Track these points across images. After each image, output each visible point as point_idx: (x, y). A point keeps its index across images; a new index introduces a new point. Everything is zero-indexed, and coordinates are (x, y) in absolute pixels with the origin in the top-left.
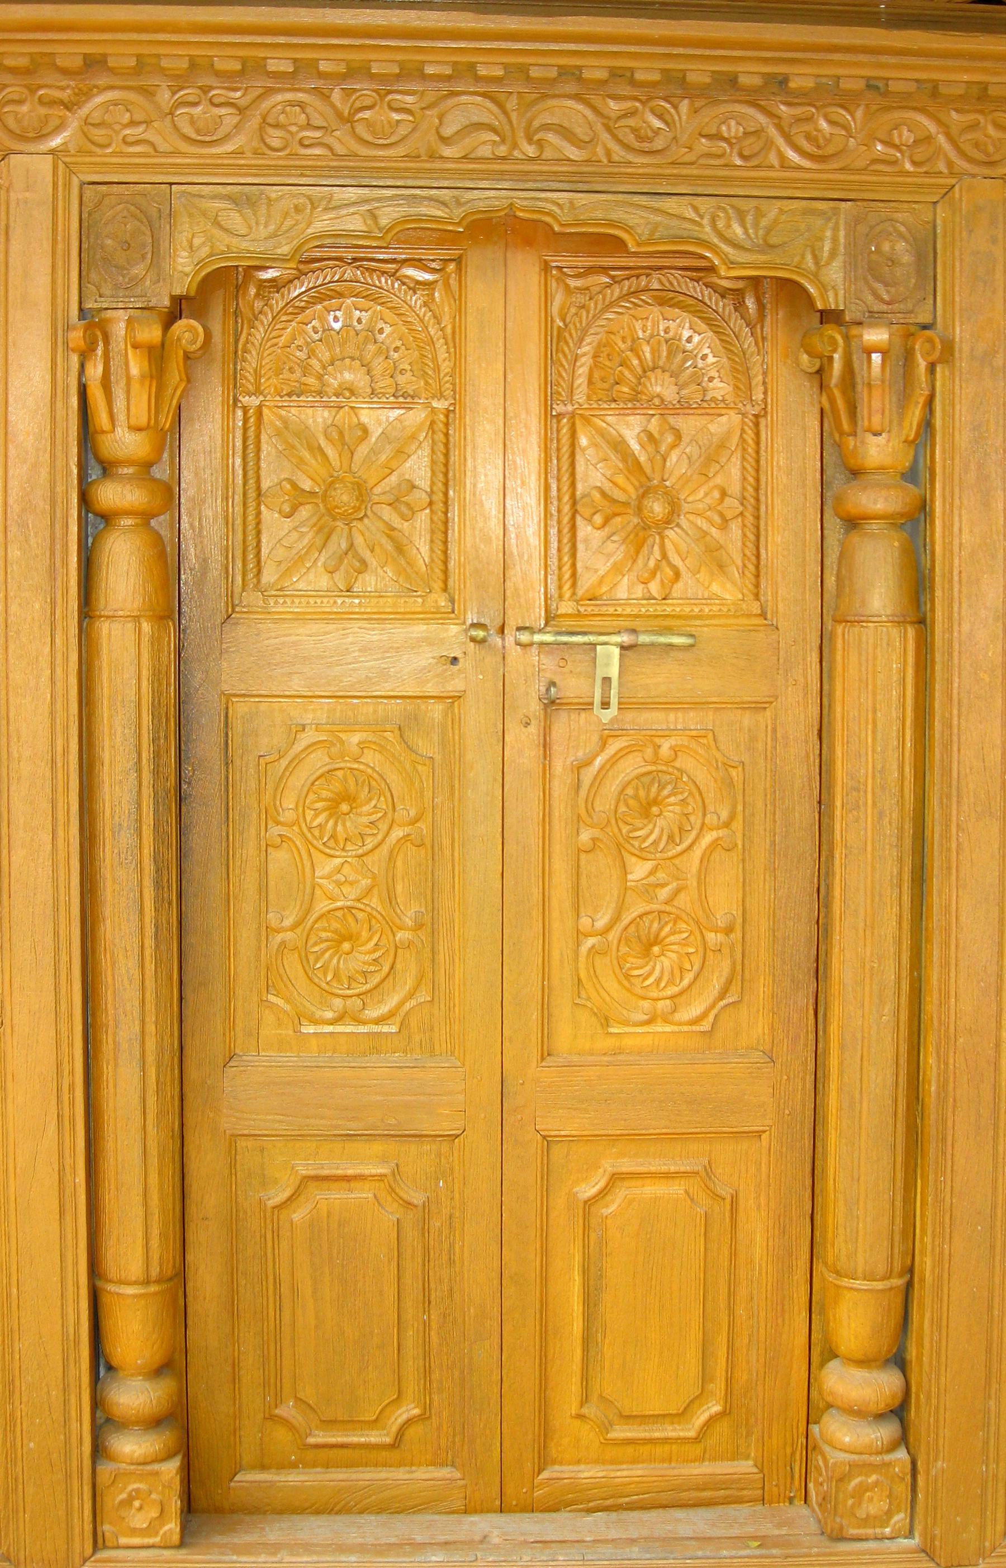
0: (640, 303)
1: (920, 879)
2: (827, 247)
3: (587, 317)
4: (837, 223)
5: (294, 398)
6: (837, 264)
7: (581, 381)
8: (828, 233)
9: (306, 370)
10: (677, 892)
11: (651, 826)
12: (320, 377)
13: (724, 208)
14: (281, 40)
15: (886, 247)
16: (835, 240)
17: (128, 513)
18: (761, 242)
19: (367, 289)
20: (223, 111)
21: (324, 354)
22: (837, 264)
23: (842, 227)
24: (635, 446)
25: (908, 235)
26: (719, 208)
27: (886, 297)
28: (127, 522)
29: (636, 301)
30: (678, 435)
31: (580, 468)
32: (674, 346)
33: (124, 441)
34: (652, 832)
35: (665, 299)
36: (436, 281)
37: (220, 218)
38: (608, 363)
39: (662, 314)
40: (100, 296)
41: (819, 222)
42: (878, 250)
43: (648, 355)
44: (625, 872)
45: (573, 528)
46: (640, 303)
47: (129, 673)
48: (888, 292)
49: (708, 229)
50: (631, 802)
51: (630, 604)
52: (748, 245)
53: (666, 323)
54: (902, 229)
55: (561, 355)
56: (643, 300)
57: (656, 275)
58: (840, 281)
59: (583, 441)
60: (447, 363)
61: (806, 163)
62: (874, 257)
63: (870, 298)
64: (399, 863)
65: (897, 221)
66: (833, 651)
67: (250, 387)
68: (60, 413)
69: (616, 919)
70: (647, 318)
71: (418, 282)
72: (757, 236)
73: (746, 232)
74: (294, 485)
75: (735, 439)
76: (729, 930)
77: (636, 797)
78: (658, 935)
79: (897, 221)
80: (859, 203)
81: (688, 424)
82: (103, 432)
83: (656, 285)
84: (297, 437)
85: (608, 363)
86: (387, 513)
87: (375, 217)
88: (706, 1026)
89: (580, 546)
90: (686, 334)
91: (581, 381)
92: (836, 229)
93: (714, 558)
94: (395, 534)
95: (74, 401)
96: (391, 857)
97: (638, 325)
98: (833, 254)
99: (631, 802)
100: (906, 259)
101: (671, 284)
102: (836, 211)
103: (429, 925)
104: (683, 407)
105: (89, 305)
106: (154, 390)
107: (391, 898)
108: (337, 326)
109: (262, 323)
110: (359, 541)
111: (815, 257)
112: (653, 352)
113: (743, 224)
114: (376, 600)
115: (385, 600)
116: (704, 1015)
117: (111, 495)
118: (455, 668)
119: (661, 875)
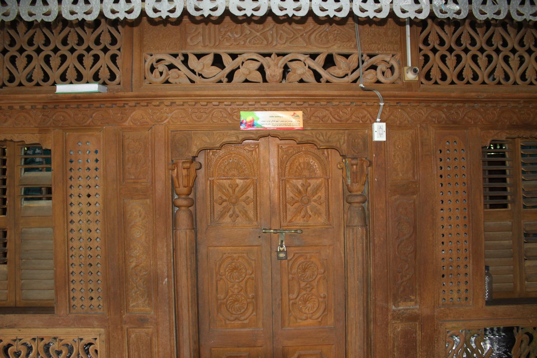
1: (198, 320)
2: (343, 141)
6: (345, 145)
10: (312, 289)
12: (227, 173)
14: (216, 98)
15: (356, 141)
16: (344, 139)
17: (183, 206)
20: (203, 114)
21: (227, 167)
22: (345, 145)
24: (300, 187)
28: (183, 208)
31: (287, 192)
32: (308, 164)
35: (307, 153)
41: (341, 135)
44: (300, 284)
45: (286, 206)
59: (288, 186)
61: (338, 122)
63: (353, 152)
66: (347, 299)
69: (298, 296)
74: (222, 198)
75: (323, 185)
76: (325, 297)
83: (304, 150)
84: (221, 187)
86: (243, 204)
87: (238, 138)
88: (320, 320)
89: (288, 210)
90: (311, 160)
92: (344, 136)
95: (170, 181)
96: (246, 282)
98: (344, 143)
100: (361, 143)
102: (345, 133)
103: (255, 297)
107: (246, 292)
108: (231, 161)
110: (237, 210)
111: (340, 143)
113: (323, 136)
116: (319, 317)
118: (259, 239)
119: (308, 286)
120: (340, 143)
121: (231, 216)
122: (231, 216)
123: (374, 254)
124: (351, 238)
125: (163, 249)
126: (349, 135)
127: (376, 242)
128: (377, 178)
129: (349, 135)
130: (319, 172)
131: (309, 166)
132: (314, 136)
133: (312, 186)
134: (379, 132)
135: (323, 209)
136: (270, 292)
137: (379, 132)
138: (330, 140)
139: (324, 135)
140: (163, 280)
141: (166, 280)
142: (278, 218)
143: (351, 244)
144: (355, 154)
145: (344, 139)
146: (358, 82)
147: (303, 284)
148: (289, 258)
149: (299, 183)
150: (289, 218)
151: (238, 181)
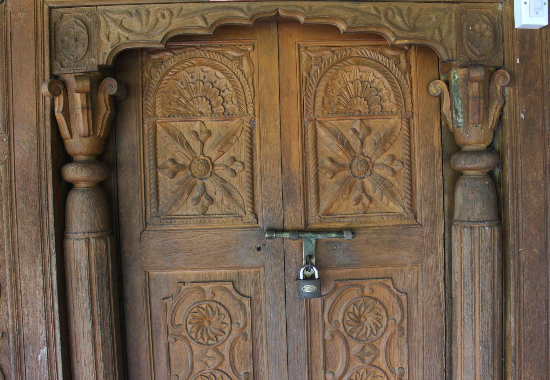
0: (347, 64)
3: (321, 72)
4: (451, 15)
5: (172, 118)
7: (319, 104)
8: (446, 20)
9: (178, 102)
11: (361, 327)
13: (392, 8)
15: (477, 27)
16: (450, 24)
18: (412, 26)
19: (209, 61)
23: (453, 16)
25: (488, 21)
26: (389, 8)
27: (478, 53)
29: (345, 63)
30: (369, 130)
33: (78, 143)
34: (362, 330)
36: (243, 56)
37: (123, 23)
38: (332, 94)
39: (359, 69)
40: (62, 67)
42: (473, 29)
43: (352, 90)
46: (347, 64)
47: (84, 264)
48: (479, 50)
49: (383, 19)
50: (350, 323)
51: (348, 217)
52: (404, 27)
53: (361, 74)
54: (485, 17)
55: (307, 91)
56: (349, 62)
57: (354, 50)
58: (454, 46)
60: (250, 97)
62: (471, 32)
63: (470, 53)
64: (236, 349)
65: (482, 13)
67: (150, 113)
68: (42, 131)
70: (351, 71)
71: (234, 57)
72: (409, 22)
73: (404, 21)
77: (354, 313)
78: (356, 321)
79: (482, 13)
80: (462, 4)
81: (374, 123)
82: (67, 139)
83: (355, 55)
85: (332, 94)
91: (319, 104)
92: (450, 17)
93: (388, 189)
94: (226, 185)
97: (347, 75)
98: (449, 32)
99: (351, 315)
100: (488, 33)
101: (363, 54)
104: (371, 114)
105: (56, 72)
106: (90, 114)
109: (155, 81)
111: (440, 32)
112: (354, 87)
113: (401, 16)
114: (218, 219)
115: (222, 219)
117: (72, 173)
118: (260, 252)
120: (440, 32)
121: (198, 201)
122: (198, 201)
123: (518, 285)
124: (466, 251)
125: (75, 247)
126: (461, 13)
127: (523, 257)
128: (526, 114)
129: (461, 13)
130: (390, 104)
131: (367, 91)
132: (382, 15)
133: (374, 132)
134: (487, 183)
135: (400, 184)
136: (285, 366)
137: (487, 183)
138: (418, 25)
139: (404, 13)
140: (36, 351)
141: (44, 350)
142: (299, 206)
143: (466, 263)
144: (475, 57)
145: (450, 24)
146: (243, 162)
147: (356, 348)
148: (324, 293)
149: (348, 127)
150: (324, 205)
151: (210, 125)
